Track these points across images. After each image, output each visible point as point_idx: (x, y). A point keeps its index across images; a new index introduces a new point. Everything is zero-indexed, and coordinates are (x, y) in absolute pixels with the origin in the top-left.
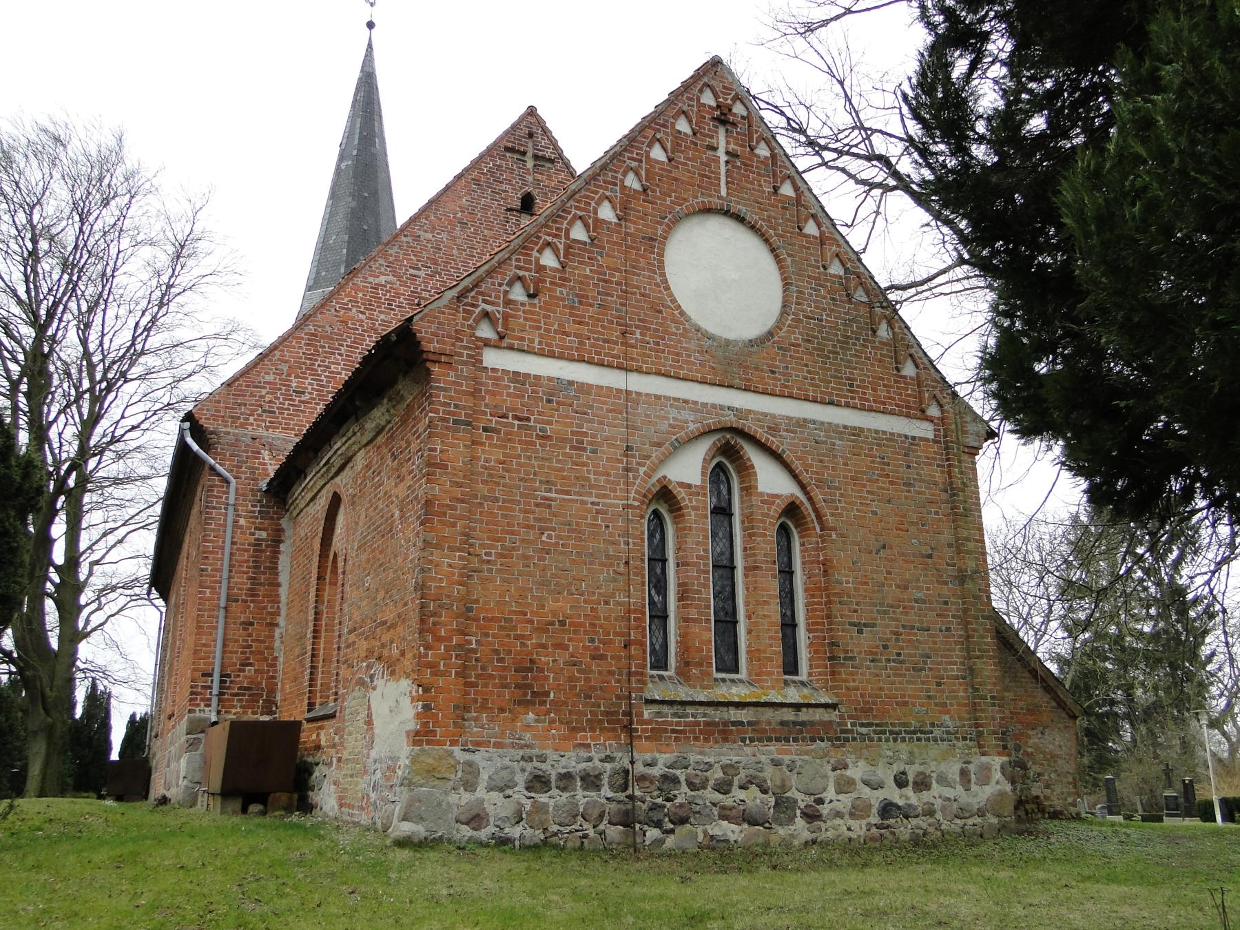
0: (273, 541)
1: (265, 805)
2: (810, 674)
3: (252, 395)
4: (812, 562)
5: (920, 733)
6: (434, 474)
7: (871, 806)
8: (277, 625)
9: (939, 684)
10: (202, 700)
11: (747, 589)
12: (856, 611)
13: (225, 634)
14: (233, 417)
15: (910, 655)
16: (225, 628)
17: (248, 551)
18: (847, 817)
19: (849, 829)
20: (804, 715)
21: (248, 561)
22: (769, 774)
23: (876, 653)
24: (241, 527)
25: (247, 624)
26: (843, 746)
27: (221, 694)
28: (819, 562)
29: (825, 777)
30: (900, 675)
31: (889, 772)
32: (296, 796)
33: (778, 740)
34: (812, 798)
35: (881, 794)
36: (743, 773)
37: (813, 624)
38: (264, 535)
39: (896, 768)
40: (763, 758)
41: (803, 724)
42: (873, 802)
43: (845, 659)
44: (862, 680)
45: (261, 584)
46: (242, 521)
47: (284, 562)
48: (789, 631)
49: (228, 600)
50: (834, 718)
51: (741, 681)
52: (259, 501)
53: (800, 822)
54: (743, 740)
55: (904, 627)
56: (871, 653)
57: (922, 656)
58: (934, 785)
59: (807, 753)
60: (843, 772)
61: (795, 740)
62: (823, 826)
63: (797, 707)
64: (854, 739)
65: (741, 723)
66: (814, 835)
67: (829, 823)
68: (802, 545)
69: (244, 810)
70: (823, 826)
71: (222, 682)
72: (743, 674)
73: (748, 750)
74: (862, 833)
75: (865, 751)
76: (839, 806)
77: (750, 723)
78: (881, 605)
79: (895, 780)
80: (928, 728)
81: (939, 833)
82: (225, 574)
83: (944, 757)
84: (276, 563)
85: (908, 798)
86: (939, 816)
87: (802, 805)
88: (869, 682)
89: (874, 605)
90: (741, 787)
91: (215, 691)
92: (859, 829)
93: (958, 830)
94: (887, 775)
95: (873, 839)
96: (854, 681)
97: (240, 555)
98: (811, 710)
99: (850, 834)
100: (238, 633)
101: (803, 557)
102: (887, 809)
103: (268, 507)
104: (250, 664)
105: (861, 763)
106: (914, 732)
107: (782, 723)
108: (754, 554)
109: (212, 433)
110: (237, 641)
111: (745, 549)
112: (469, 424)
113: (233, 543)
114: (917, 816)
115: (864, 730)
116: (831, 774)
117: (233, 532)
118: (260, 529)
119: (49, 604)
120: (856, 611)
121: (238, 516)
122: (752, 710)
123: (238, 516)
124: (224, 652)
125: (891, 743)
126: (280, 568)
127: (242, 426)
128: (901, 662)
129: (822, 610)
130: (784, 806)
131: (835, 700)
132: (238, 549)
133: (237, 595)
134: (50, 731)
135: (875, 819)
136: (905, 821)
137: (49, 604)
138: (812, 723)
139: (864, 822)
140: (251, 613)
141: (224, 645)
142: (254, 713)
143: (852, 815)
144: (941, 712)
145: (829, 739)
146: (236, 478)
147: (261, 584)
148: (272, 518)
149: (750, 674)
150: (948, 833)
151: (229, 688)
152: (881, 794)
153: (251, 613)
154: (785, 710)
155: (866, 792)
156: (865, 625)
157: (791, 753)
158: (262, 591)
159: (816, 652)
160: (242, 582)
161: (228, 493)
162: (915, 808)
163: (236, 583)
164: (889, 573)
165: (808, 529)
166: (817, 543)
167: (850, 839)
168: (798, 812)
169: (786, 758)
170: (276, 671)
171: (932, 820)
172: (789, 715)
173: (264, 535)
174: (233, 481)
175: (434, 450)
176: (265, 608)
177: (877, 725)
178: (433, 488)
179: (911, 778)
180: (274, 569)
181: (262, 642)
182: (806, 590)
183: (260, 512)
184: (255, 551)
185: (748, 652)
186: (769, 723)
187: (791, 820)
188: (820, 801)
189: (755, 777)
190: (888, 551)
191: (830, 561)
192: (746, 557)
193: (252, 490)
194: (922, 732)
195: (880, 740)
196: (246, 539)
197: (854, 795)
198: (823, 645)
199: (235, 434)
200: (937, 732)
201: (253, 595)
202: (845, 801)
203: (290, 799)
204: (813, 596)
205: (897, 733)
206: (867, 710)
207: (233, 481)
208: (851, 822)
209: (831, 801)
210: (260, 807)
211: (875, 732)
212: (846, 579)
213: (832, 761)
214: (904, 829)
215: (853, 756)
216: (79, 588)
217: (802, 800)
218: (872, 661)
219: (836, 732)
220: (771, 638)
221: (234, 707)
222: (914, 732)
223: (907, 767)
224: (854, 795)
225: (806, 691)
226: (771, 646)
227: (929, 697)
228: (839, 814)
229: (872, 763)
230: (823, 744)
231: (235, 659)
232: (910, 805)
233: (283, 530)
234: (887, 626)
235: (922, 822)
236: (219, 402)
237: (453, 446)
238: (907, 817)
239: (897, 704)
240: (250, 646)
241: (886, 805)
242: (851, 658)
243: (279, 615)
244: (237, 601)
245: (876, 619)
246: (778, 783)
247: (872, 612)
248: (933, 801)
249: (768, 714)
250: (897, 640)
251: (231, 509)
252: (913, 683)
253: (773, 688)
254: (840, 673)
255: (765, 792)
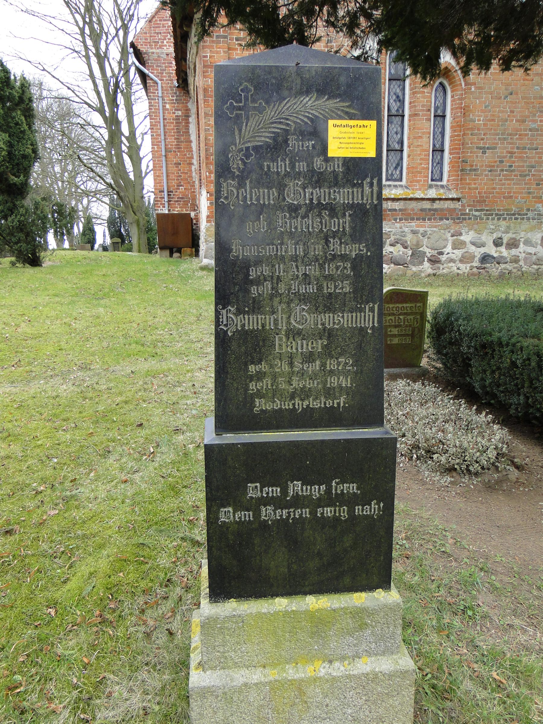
0: (185, 116)
1: (180, 253)
2: (448, 181)
3: (164, 27)
4: (457, 108)
5: (518, 215)
6: (207, 72)
7: (474, 257)
8: (193, 164)
9: (538, 185)
10: (161, 204)
11: (410, 129)
12: (482, 139)
13: (167, 170)
14: (155, 42)
15: (519, 166)
16: (167, 167)
17: (173, 123)
18: (458, 262)
19: (458, 269)
20: (437, 205)
21: (174, 129)
22: (409, 238)
23: (494, 166)
24: (168, 110)
25: (178, 164)
26: (461, 223)
27: (169, 201)
28: (461, 108)
29: (447, 240)
30: (509, 180)
31: (490, 238)
32: (194, 250)
33: (417, 219)
34: (436, 251)
35: (482, 250)
36: (392, 238)
37: (453, 149)
38: (180, 113)
39: (495, 236)
40: (406, 230)
41: (436, 210)
42: (476, 254)
43: (470, 170)
44: (481, 183)
45: (182, 142)
46: (168, 106)
47: (193, 128)
48: (438, 154)
49: (166, 152)
50: (457, 206)
51: (401, 186)
52: (175, 93)
53: (426, 264)
54: (395, 220)
55: (518, 148)
56: (490, 166)
57: (528, 166)
58: (522, 245)
59: (435, 227)
60: (459, 237)
61: (429, 219)
62: (441, 267)
63: (433, 200)
64: (470, 219)
65: (395, 210)
66: (435, 272)
67: (445, 265)
68: (452, 97)
69: (171, 256)
70: (441, 267)
71: (168, 195)
72: (404, 183)
73: (398, 225)
74: (466, 271)
75: (476, 226)
76: (453, 256)
77: (400, 210)
78: (503, 134)
79: (494, 242)
80: (525, 212)
81: (520, 273)
82: (163, 138)
83: (532, 229)
84: (188, 129)
85: (501, 252)
86: (522, 263)
87: (429, 255)
88: (485, 184)
89: (498, 134)
90: (391, 245)
91: (166, 199)
92: (465, 268)
93: (533, 271)
94: (488, 239)
95: (473, 274)
96: (475, 184)
97: (170, 126)
98: (442, 202)
99: (459, 271)
100: (173, 169)
101: (452, 105)
102: (485, 258)
103: (180, 96)
104: (181, 186)
105: (472, 233)
106: (514, 214)
107: (422, 210)
108: (415, 106)
109: (145, 53)
110: (174, 173)
111: (410, 103)
112: (226, 37)
113: (164, 119)
114: (506, 263)
115: (477, 213)
116: (450, 238)
117: (163, 113)
118: (178, 110)
119: (126, 158)
120: (482, 139)
121: (165, 103)
122: (402, 203)
123: (165, 103)
124: (167, 180)
125: (495, 221)
126: (191, 132)
127: (161, 47)
128: (512, 171)
129: (460, 140)
130: (417, 256)
131: (460, 196)
132: (168, 123)
133: (170, 148)
134: (138, 223)
135: (476, 264)
136: (497, 265)
137: (126, 158)
138: (442, 210)
139: (469, 265)
140: (179, 158)
141: (167, 176)
142: (186, 210)
143: (461, 261)
144: (536, 202)
145: (453, 219)
146: (161, 80)
147: (182, 142)
148: (183, 103)
149: (407, 182)
150: (526, 272)
151: (173, 198)
152: (482, 250)
153: (179, 158)
154: (424, 202)
155: (473, 248)
156: (488, 148)
157: (426, 227)
158: (183, 145)
159: (453, 167)
160: (172, 141)
161: (157, 90)
162: (506, 258)
163: (169, 142)
164: (512, 112)
165: (457, 85)
166: (462, 95)
167: (458, 274)
168: (426, 259)
169: (422, 230)
170: (195, 189)
171: (516, 265)
172: (427, 205)
173: (180, 113)
174: (159, 82)
175: (206, 57)
176: (185, 155)
177: (487, 210)
178: (207, 81)
179: (505, 241)
180: (187, 133)
181: (187, 173)
182: (452, 127)
183: (176, 100)
184: (176, 123)
185: (407, 168)
186: (413, 210)
187: (421, 263)
188: (441, 253)
189: (401, 240)
190: (514, 96)
191: (469, 107)
192: (410, 108)
193: (171, 87)
194: (519, 214)
195: (488, 219)
196: (170, 116)
197: (464, 250)
198: (458, 162)
199: (157, 53)
200: (530, 214)
201: (178, 148)
202: (458, 253)
203: (192, 251)
204: (455, 131)
205: (501, 215)
206: (482, 201)
207: (159, 82)
208: (460, 265)
209: (448, 253)
210: (178, 254)
211: (485, 215)
212: (478, 119)
213: (452, 231)
214: (495, 270)
215: (467, 229)
216: (139, 148)
217: (429, 252)
218: (490, 171)
219: (457, 214)
220: (421, 159)
221: (177, 207)
222: (514, 214)
223: (503, 235)
224: (464, 250)
225: (442, 191)
226: (421, 164)
227: (529, 193)
228: (452, 261)
229: (479, 232)
230: (447, 222)
231: (174, 183)
232: (502, 257)
233: (189, 110)
234: (505, 148)
235: (509, 266)
236: (146, 33)
237: (217, 52)
238: (499, 263)
239: (504, 197)
240: (181, 176)
241: (485, 256)
242: (475, 170)
243: (193, 158)
244: (171, 152)
245: (497, 144)
246: (415, 243)
247: (495, 139)
248: (518, 254)
249: (413, 204)
250: (512, 157)
251: (160, 99)
252: (518, 184)
253: (420, 190)
254: (465, 179)
255: (406, 248)
